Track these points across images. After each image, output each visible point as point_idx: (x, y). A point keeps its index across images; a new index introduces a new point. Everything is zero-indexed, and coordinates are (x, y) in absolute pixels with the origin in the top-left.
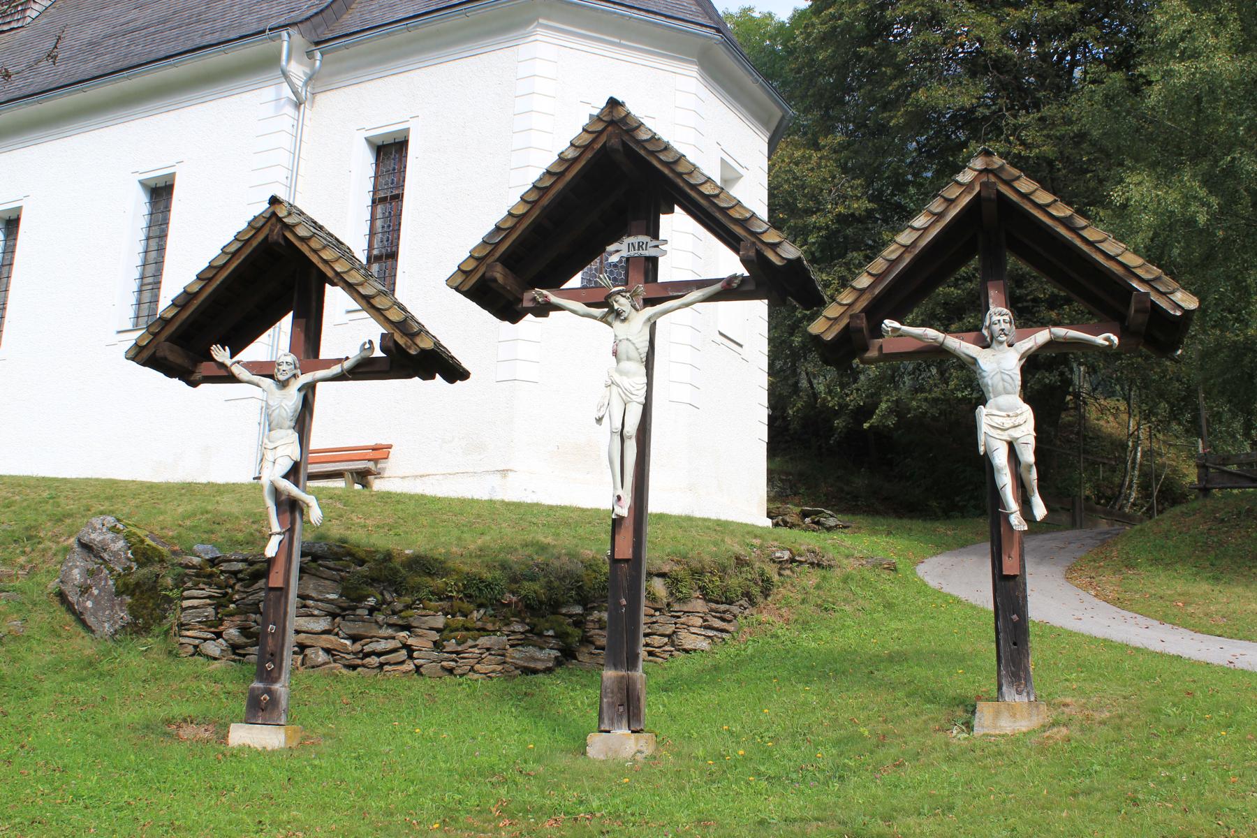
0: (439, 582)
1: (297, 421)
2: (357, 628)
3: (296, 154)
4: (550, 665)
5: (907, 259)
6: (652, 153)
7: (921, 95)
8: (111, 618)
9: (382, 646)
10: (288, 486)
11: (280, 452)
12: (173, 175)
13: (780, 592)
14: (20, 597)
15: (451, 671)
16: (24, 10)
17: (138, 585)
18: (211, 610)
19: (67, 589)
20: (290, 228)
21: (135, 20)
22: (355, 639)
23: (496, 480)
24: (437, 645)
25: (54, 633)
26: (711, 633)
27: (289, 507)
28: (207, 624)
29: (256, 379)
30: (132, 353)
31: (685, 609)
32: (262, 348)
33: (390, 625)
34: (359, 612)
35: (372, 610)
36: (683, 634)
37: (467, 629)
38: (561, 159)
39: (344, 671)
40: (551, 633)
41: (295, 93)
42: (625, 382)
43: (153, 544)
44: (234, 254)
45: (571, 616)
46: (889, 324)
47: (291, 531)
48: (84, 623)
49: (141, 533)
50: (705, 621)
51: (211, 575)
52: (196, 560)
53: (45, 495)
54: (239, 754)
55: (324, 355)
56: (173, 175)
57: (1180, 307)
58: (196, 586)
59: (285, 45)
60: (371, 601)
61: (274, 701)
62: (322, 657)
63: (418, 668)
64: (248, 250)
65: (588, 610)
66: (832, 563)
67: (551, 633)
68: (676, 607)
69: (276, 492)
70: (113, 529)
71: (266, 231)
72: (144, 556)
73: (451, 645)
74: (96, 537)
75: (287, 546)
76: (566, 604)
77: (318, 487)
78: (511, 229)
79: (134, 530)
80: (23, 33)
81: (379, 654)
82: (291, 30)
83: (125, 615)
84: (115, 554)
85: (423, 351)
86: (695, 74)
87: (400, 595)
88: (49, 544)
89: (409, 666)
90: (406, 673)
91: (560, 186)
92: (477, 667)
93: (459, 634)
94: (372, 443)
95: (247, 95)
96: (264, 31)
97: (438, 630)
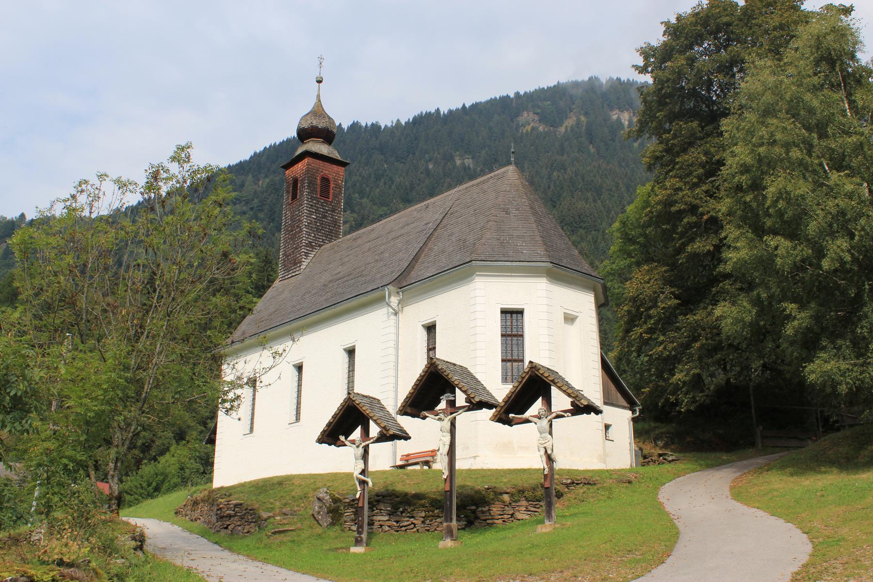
0: (423, 501)
1: (363, 457)
2: (398, 518)
3: (398, 335)
4: (463, 527)
5: (513, 396)
6: (442, 372)
7: (689, 249)
8: (326, 521)
9: (406, 523)
10: (362, 477)
11: (358, 467)
12: (354, 346)
13: (565, 497)
14: (301, 517)
15: (428, 530)
16: (300, 266)
17: (333, 510)
18: (353, 516)
19: (314, 513)
20: (354, 401)
21: (340, 272)
22: (397, 522)
23: (472, 460)
24: (423, 522)
25: (311, 527)
26: (529, 513)
27: (363, 483)
28: (353, 520)
29: (351, 445)
30: (503, 310)
31: (517, 504)
32: (353, 437)
33: (408, 517)
34: (398, 513)
35: (402, 512)
36: (517, 514)
37: (433, 516)
38: (421, 376)
39: (395, 533)
40: (463, 516)
41: (394, 310)
42: (444, 439)
43: (338, 496)
44: (343, 406)
45: (471, 510)
46: (511, 415)
47: (364, 490)
48: (319, 523)
49: (334, 493)
50: (527, 508)
51: (352, 505)
52: (347, 500)
53: (312, 481)
54: (355, 554)
55: (370, 436)
56: (354, 346)
57: (583, 404)
58: (348, 509)
59: (387, 292)
60: (401, 509)
61: (362, 540)
62: (387, 528)
63: (418, 530)
64: (344, 409)
65: (478, 507)
66: (596, 482)
67: (463, 516)
68: (514, 504)
69: (357, 478)
70: (326, 492)
71: (348, 402)
72: (335, 500)
73: (428, 522)
74: (321, 495)
75: (362, 494)
76: (468, 506)
77: (414, 469)
78: (410, 397)
79: (332, 492)
80: (300, 277)
81: (405, 526)
82: (388, 286)
83: (330, 520)
84: (327, 500)
85: (391, 435)
86: (545, 281)
87: (410, 507)
88: (311, 499)
89: (415, 530)
90: (414, 532)
91: (421, 383)
92: (437, 529)
93: (430, 518)
94: (431, 449)
95: (378, 311)
96: (379, 288)
97: (423, 517)
